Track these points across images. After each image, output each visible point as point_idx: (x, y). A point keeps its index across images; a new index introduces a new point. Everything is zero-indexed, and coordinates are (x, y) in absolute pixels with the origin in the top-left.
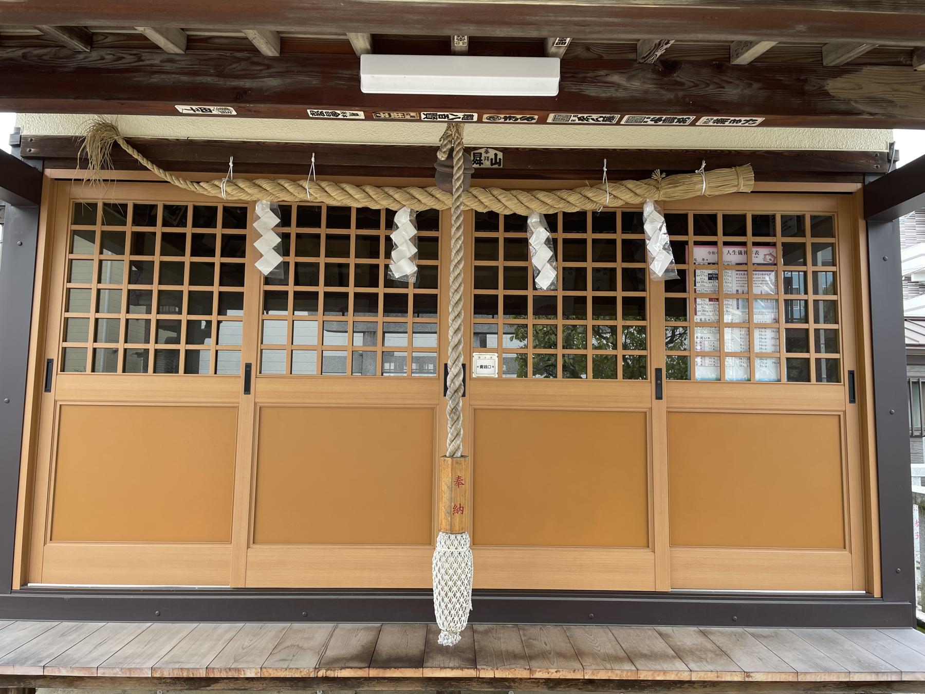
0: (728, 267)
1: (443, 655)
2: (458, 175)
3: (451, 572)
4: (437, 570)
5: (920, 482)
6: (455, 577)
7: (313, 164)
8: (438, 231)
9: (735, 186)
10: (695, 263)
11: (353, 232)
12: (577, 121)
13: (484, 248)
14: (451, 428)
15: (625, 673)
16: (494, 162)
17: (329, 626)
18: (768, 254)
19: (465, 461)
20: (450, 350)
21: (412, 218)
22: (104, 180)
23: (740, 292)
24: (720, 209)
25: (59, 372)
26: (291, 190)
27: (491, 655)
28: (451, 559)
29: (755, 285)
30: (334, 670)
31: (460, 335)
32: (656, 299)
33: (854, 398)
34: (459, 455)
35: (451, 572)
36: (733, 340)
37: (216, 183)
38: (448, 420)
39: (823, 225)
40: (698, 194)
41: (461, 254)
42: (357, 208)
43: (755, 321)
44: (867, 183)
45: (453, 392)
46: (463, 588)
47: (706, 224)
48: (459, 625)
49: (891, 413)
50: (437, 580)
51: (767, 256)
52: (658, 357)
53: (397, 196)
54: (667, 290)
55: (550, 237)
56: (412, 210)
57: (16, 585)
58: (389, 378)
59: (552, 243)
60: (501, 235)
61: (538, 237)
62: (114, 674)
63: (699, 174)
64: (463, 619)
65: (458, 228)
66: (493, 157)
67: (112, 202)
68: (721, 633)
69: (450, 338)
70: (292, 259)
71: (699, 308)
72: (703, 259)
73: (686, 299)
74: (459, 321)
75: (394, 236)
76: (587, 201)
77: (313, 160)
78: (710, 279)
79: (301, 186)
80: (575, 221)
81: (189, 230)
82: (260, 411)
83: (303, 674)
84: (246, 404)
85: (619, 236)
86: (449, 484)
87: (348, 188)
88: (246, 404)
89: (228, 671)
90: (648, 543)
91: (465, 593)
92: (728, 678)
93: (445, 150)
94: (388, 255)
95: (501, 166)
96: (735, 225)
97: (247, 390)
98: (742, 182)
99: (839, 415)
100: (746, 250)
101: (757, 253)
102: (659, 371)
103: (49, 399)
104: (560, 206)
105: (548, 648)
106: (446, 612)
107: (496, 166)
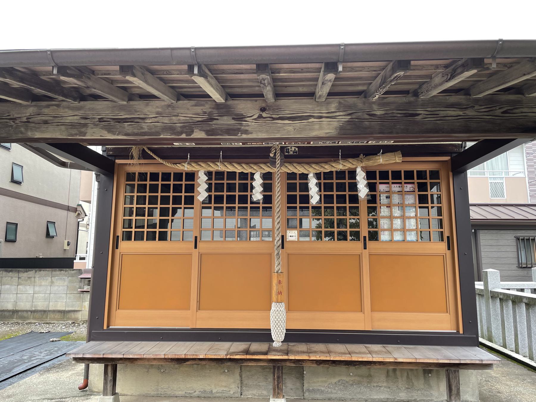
0: (394, 193)
1: (275, 352)
2: (278, 162)
3: (277, 317)
4: (272, 317)
5: (530, 291)
6: (279, 319)
7: (221, 155)
8: (272, 180)
9: (394, 160)
10: (380, 192)
11: (237, 182)
12: (322, 143)
13: (291, 187)
14: (276, 261)
15: (346, 358)
16: (294, 152)
17: (230, 343)
18: (411, 187)
19: (282, 274)
20: (276, 230)
21: (261, 176)
22: (139, 164)
23: (400, 203)
24: (390, 169)
25: (121, 241)
26: (213, 166)
27: (294, 352)
28: (277, 312)
29: (406, 200)
30: (233, 356)
31: (279, 225)
32: (363, 207)
33: (450, 248)
34: (280, 272)
35: (277, 317)
36: (397, 223)
37: (183, 164)
38: (275, 258)
39: (435, 175)
40: (379, 163)
41: (280, 193)
42: (239, 173)
43: (406, 215)
44: (452, 156)
45: (277, 247)
46: (282, 324)
47: (384, 175)
48: (281, 338)
49: (465, 254)
50: (272, 321)
51: (411, 188)
52: (364, 231)
53: (255, 168)
54: (368, 203)
55: (318, 182)
56: (261, 173)
57: (105, 328)
58: (254, 241)
59: (319, 185)
60: (298, 181)
61: (313, 182)
62: (150, 357)
63: (379, 155)
64: (282, 336)
65: (278, 183)
66: (294, 150)
67: (142, 172)
68: (392, 347)
69: (276, 226)
71: (382, 210)
72: (384, 190)
73: (376, 207)
74: (279, 219)
75: (254, 184)
76: (333, 167)
77: (221, 153)
78: (386, 198)
79: (217, 164)
80: (328, 175)
82: (201, 256)
83: (221, 357)
84: (195, 253)
85: (347, 181)
86: (276, 283)
87: (235, 165)
88: (195, 253)
89: (193, 355)
91: (283, 326)
92: (388, 360)
93: (273, 153)
94: (251, 191)
95: (297, 154)
96: (396, 175)
98: (397, 158)
99: (360, 255)
100: (401, 185)
101: (406, 187)
102: (365, 237)
103: (118, 252)
104: (322, 170)
105: (318, 350)
106: (276, 333)
107: (295, 154)
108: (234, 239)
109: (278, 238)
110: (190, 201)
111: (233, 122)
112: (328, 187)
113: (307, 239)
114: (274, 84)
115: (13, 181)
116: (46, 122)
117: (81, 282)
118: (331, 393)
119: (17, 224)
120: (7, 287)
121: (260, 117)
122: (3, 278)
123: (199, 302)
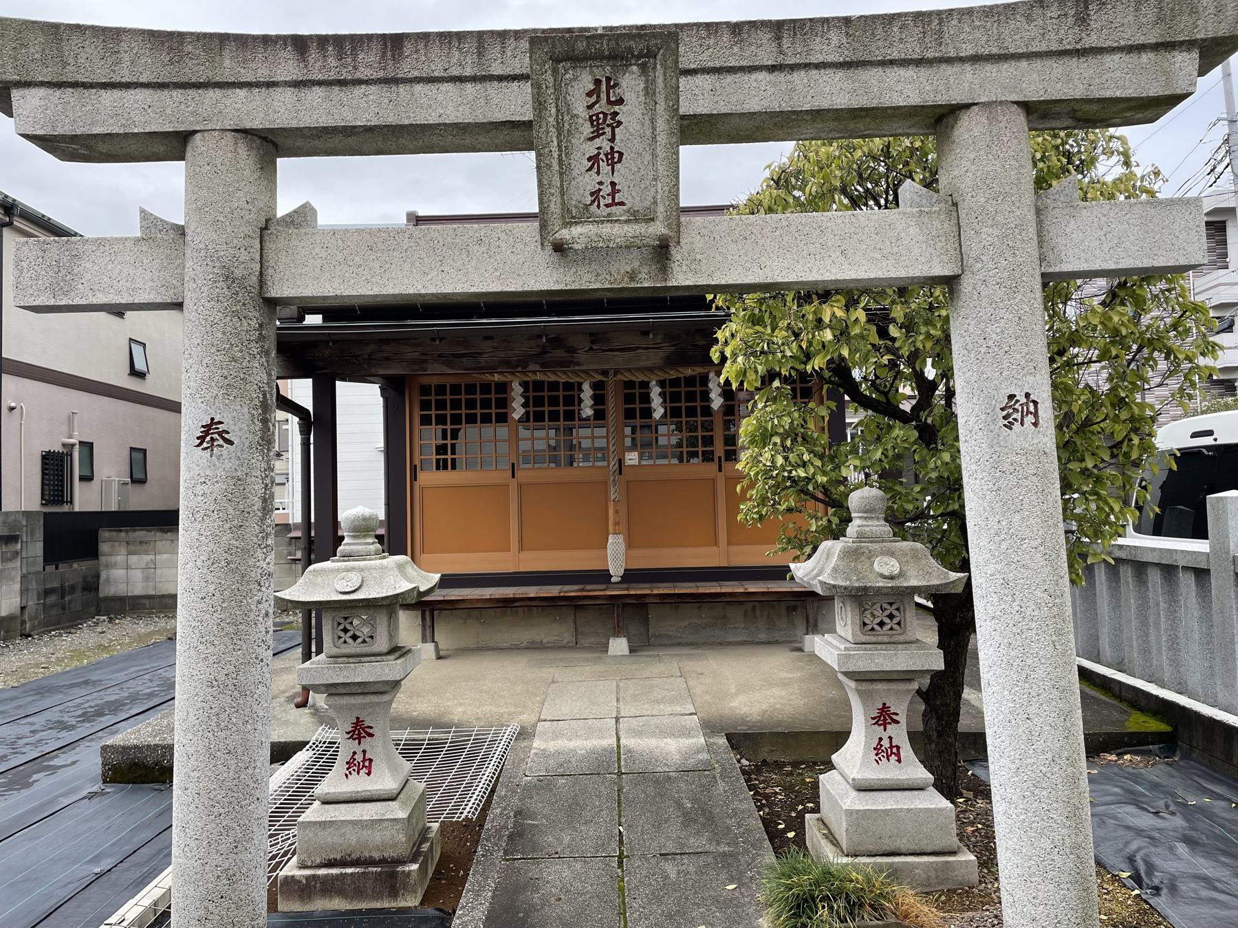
11: (561, 393)
13: (629, 399)
59: (663, 395)
61: (655, 392)
70: (531, 409)
80: (675, 382)
81: (448, 397)
82: (520, 486)
84: (513, 484)
90: (716, 544)
94: (579, 405)
97: (513, 477)
102: (720, 458)
103: (417, 484)
108: (545, 465)
109: (613, 463)
110: (503, 418)
111: (565, 354)
112: (675, 397)
113: (665, 462)
114: (604, 379)
115: (135, 373)
116: (387, 359)
117: (290, 544)
118: (681, 637)
119: (145, 450)
120: (165, 556)
121: (591, 349)
122: (158, 543)
123: (521, 541)
